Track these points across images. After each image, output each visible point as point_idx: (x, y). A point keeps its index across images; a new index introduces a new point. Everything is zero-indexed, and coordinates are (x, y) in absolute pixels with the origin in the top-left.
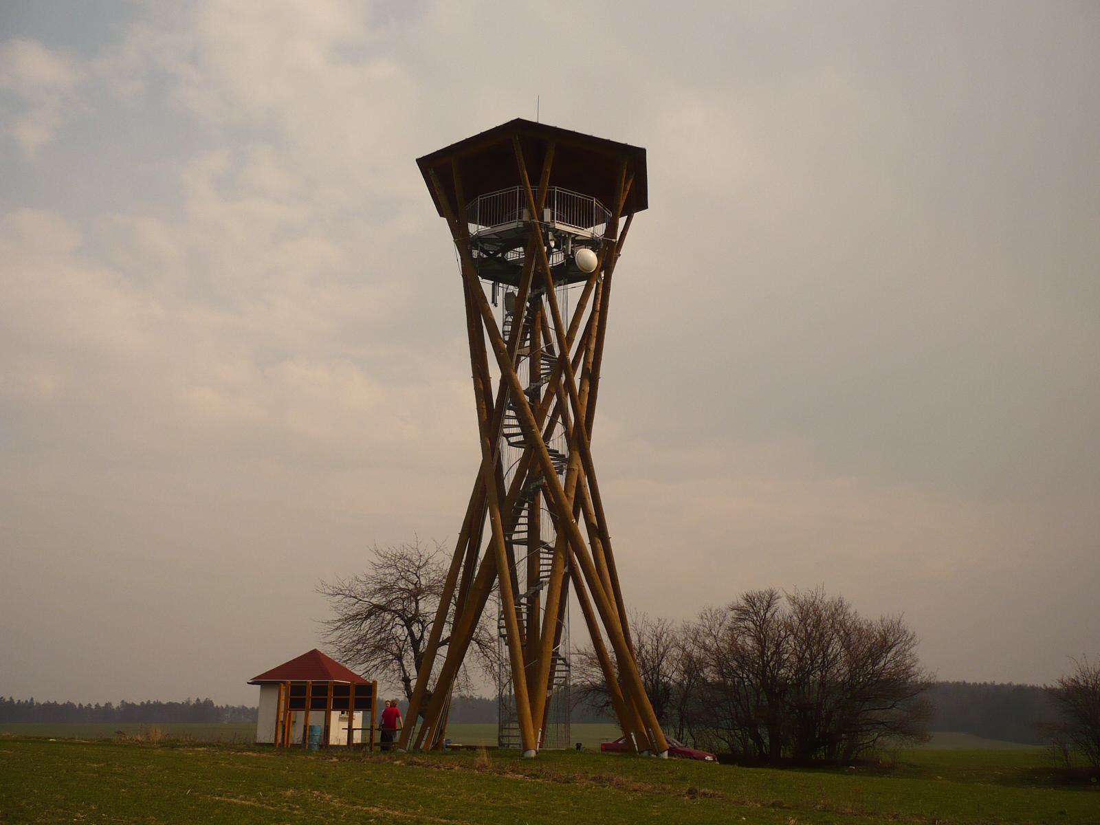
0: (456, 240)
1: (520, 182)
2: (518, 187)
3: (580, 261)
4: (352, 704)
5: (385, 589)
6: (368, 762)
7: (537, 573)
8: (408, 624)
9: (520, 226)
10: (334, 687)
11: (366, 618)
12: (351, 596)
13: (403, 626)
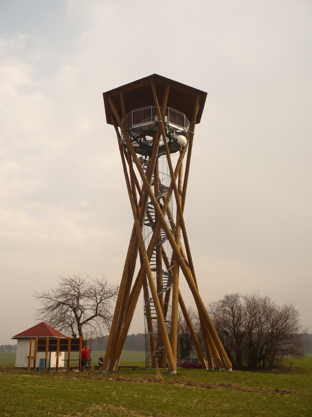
0: (122, 130)
1: (153, 103)
2: (152, 106)
3: (180, 141)
4: (58, 348)
5: (65, 295)
6: (94, 379)
7: (162, 284)
8: (75, 310)
9: (153, 124)
10: (60, 340)
11: (56, 308)
12: (49, 298)
13: (71, 311)
